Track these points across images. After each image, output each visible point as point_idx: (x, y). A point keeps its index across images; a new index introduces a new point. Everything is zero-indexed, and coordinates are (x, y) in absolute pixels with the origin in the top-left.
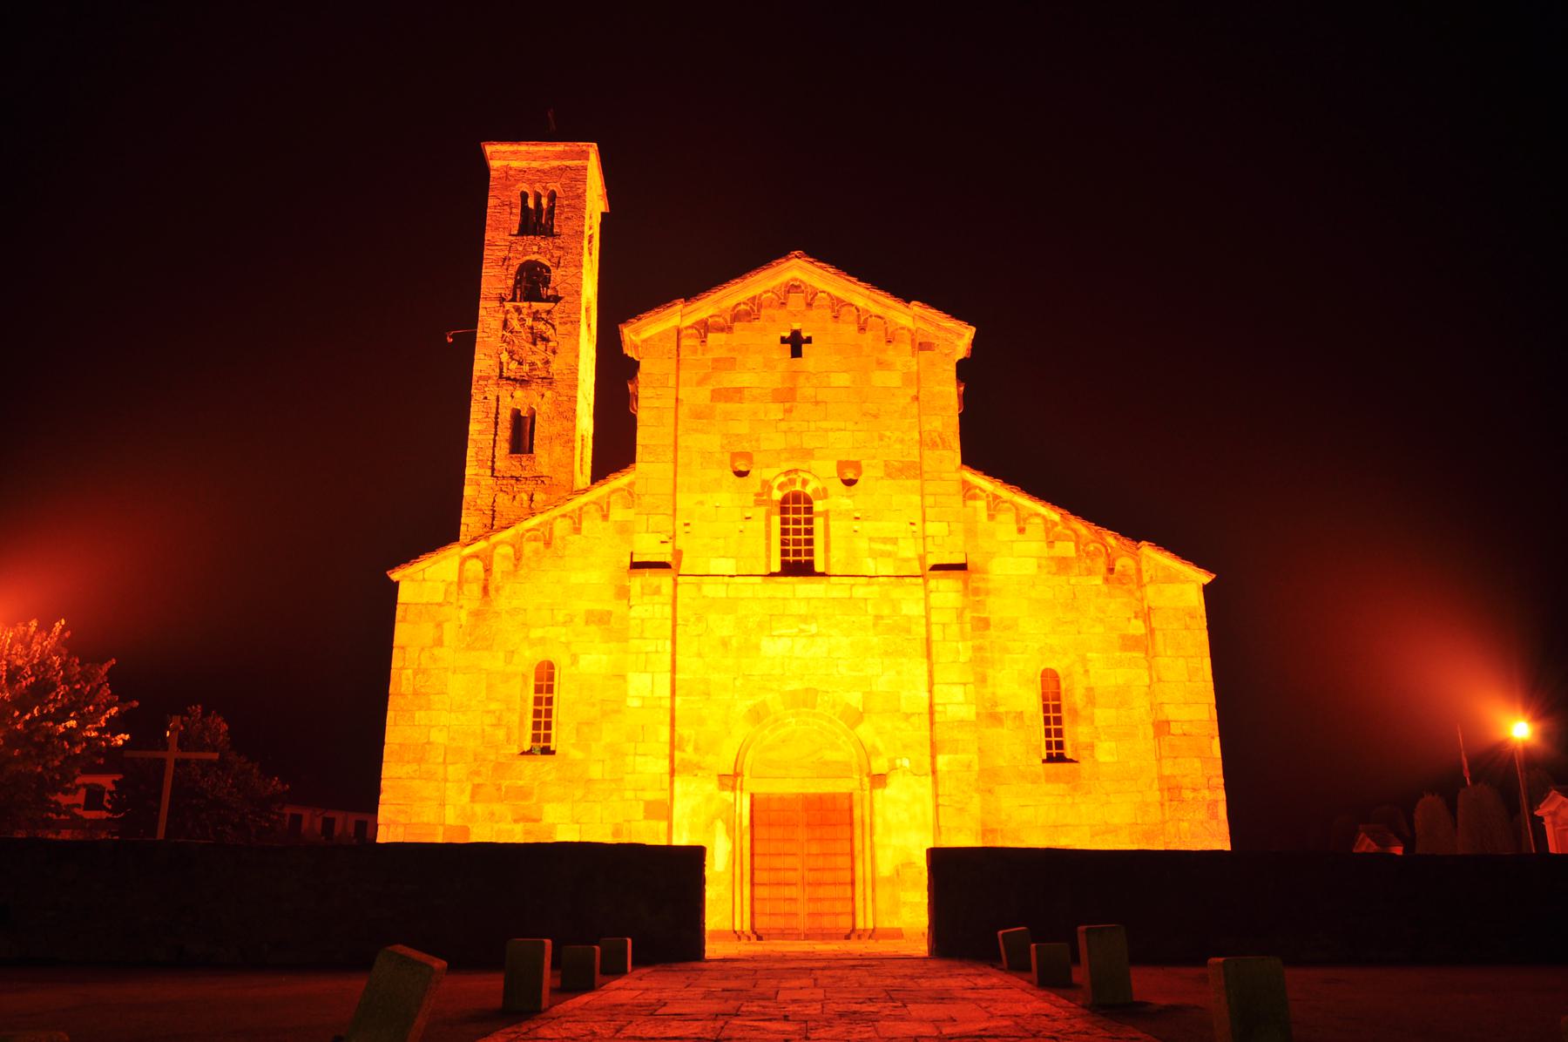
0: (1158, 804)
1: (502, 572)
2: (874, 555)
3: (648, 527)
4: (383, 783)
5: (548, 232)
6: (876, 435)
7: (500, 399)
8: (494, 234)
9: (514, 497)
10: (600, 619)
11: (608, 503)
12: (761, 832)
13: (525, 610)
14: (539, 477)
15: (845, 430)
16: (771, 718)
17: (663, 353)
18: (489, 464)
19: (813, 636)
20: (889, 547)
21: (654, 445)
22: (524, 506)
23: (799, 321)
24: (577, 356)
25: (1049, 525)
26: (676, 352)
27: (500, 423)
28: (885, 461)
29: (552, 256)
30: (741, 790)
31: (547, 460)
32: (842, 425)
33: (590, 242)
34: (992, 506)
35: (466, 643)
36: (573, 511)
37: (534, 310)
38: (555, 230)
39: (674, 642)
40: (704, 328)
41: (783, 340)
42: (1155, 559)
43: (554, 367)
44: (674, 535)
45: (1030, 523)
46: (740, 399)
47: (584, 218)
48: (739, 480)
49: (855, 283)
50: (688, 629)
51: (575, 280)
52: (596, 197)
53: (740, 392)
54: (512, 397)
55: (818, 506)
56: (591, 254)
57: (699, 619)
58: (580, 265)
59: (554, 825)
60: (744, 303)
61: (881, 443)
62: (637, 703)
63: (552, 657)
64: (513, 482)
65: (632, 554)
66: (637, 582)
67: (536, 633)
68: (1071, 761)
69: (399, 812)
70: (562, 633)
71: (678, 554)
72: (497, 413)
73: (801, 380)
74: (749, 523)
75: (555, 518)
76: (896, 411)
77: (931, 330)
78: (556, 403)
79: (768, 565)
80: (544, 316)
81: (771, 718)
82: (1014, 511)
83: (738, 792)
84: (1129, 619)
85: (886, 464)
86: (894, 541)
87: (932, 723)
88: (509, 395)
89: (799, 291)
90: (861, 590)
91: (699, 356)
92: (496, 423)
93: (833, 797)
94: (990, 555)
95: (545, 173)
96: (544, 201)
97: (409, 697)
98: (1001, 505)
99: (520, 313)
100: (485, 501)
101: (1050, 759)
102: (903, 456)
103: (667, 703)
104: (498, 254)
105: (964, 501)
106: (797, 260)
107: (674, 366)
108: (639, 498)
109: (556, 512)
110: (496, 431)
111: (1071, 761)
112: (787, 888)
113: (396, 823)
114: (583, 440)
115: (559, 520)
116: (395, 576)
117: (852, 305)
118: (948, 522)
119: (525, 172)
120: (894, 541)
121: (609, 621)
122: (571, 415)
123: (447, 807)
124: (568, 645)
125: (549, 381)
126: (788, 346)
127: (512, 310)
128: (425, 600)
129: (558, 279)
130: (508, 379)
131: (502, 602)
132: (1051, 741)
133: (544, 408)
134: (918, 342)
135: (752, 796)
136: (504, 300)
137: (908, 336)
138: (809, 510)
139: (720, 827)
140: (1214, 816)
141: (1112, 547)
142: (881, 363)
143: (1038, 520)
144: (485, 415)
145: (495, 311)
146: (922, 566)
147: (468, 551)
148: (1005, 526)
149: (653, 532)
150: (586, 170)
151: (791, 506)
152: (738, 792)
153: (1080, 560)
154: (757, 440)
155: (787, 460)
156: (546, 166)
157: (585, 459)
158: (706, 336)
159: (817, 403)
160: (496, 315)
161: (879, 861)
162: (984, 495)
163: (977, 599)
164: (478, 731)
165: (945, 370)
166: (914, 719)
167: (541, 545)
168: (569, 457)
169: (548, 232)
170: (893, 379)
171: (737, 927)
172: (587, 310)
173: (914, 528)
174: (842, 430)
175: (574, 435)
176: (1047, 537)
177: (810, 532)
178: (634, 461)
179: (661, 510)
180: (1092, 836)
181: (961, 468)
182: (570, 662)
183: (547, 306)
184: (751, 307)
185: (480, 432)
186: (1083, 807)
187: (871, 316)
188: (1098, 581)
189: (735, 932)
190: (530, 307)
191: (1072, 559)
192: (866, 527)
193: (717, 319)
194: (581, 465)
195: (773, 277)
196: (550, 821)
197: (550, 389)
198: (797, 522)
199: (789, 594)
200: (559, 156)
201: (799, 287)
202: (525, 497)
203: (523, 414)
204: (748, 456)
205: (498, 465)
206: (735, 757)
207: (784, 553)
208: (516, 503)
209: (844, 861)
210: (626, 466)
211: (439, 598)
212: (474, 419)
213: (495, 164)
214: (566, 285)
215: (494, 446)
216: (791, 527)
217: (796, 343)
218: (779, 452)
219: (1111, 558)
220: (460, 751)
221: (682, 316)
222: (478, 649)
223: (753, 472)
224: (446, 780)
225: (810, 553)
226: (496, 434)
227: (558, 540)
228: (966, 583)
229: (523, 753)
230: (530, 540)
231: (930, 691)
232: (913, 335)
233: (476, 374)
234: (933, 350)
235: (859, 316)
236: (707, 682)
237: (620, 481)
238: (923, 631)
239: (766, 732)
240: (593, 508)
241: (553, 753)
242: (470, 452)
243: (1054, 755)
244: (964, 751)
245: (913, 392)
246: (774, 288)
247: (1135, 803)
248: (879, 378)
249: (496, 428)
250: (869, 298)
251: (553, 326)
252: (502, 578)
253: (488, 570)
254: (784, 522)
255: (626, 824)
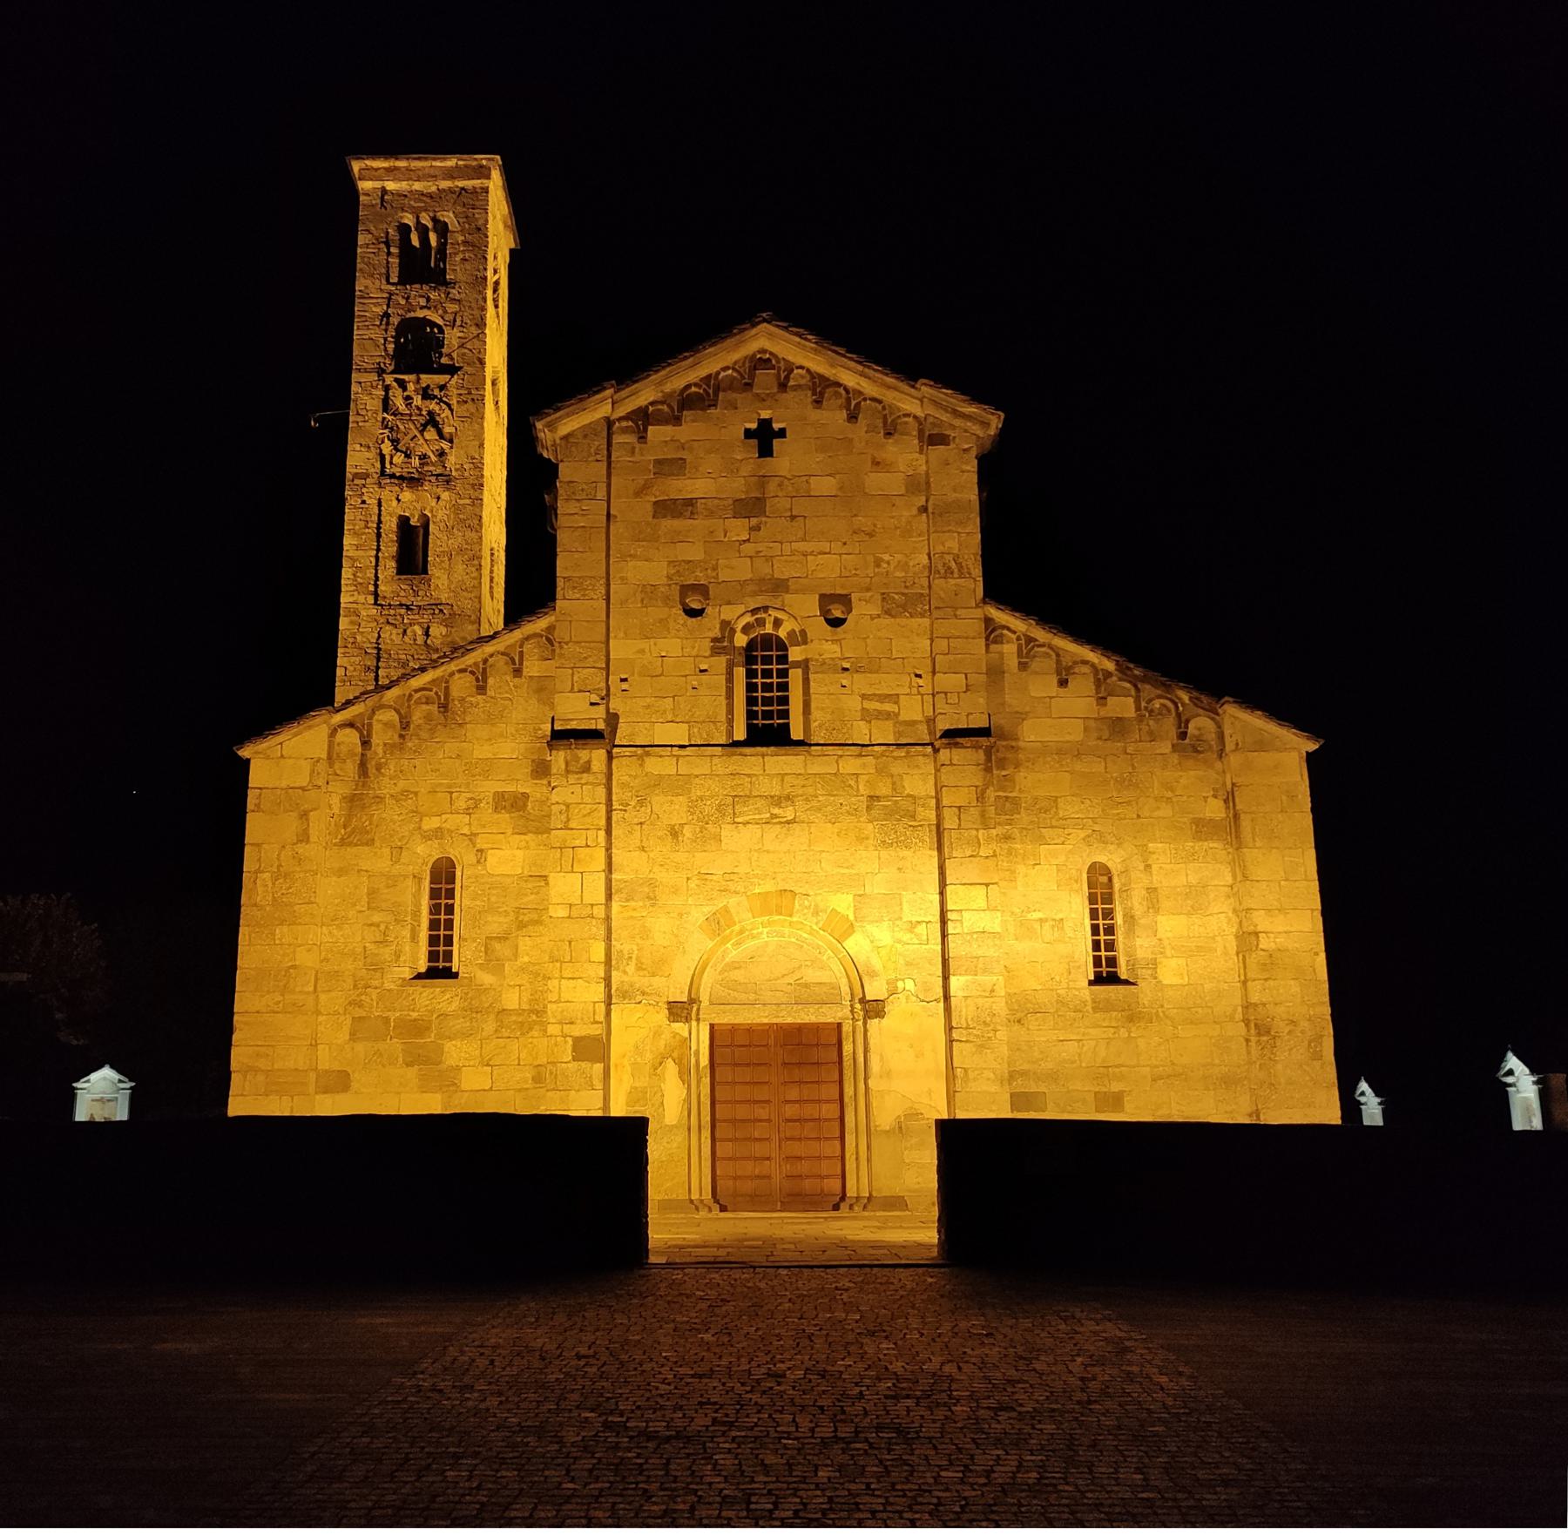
0: (1242, 1040)
1: (385, 745)
2: (867, 716)
3: (573, 685)
4: (236, 1018)
5: (438, 278)
6: (870, 559)
7: (383, 504)
8: (368, 282)
9: (405, 631)
10: (513, 803)
11: (521, 653)
12: (724, 1074)
13: (416, 794)
14: (436, 605)
15: (829, 553)
16: (737, 928)
17: (590, 455)
18: (372, 588)
19: (788, 822)
20: (888, 707)
21: (580, 578)
22: (418, 642)
23: (769, 408)
24: (482, 446)
25: (1101, 676)
26: (606, 452)
27: (383, 535)
28: (884, 594)
29: (445, 312)
30: (698, 1020)
31: (446, 583)
32: (826, 546)
33: (495, 290)
34: (1025, 651)
35: (339, 837)
36: (476, 664)
37: (424, 385)
38: (448, 277)
39: (609, 832)
40: (642, 419)
41: (749, 434)
42: (1241, 721)
43: (452, 460)
44: (608, 695)
45: (1074, 673)
46: (692, 513)
47: (486, 259)
48: (692, 621)
49: (844, 356)
50: (626, 815)
51: (477, 343)
52: (501, 226)
53: (692, 505)
54: (399, 500)
55: (795, 654)
56: (497, 307)
57: (641, 803)
58: (481, 324)
59: (458, 1068)
60: (696, 385)
61: (876, 570)
62: (562, 912)
63: (453, 853)
64: (403, 611)
65: (553, 718)
66: (559, 758)
67: (430, 823)
68: (1127, 982)
69: (258, 1055)
70: (460, 822)
71: (613, 719)
72: (380, 522)
73: (772, 487)
74: (704, 677)
75: (452, 674)
76: (896, 528)
77: (945, 417)
78: (457, 508)
79: (730, 733)
80: (436, 392)
81: (737, 928)
82: (1054, 656)
83: (694, 1023)
84: (1205, 798)
85: (885, 597)
86: (894, 698)
87: (944, 935)
88: (393, 498)
89: (769, 365)
90: (850, 765)
91: (637, 458)
92: (379, 535)
93: (816, 1029)
94: (1021, 716)
95: (432, 197)
96: (433, 238)
97: (268, 909)
98: (1036, 649)
99: (405, 389)
100: (367, 636)
101: (1099, 980)
102: (906, 587)
103: (600, 912)
104: (374, 309)
105: (987, 646)
106: (765, 324)
107: (604, 472)
108: (561, 648)
109: (453, 667)
110: (378, 546)
111: (1127, 982)
112: (757, 1145)
113: (256, 1070)
114: (492, 554)
115: (457, 676)
116: (244, 753)
117: (839, 385)
118: (966, 674)
119: (405, 196)
120: (894, 698)
121: (525, 805)
122: (475, 524)
123: (320, 1047)
124: (472, 837)
125: (446, 480)
126: (754, 442)
127: (395, 384)
128: (284, 784)
129: (455, 343)
130: (392, 476)
131: (385, 786)
132: (1099, 940)
133: (441, 515)
134: (927, 434)
135: (712, 1026)
136: (383, 371)
137: (913, 426)
138: (783, 659)
139: (671, 1068)
140: (1317, 1056)
141: (1183, 705)
142: (878, 463)
143: (1086, 669)
144: (363, 524)
145: (372, 387)
146: (931, 732)
147: (338, 718)
148: (1043, 685)
149: (580, 691)
150: (487, 192)
151: (758, 653)
152: (694, 1023)
153: (1141, 721)
154: (715, 569)
155: (754, 594)
156: (434, 189)
157: (495, 580)
158: (646, 430)
159: (793, 518)
160: (374, 391)
161: (875, 1111)
162: (1014, 637)
163: (1004, 773)
164: (359, 950)
165: (963, 472)
166: (921, 929)
167: (434, 708)
168: (474, 578)
169: (438, 278)
170: (892, 483)
171: (695, 1196)
172: (494, 383)
173: (921, 682)
174: (826, 553)
175: (480, 550)
176: (1097, 693)
177: (784, 687)
178: (554, 599)
179: (590, 661)
180: (1154, 1080)
181: (984, 601)
182: (474, 860)
183: (441, 379)
184: (705, 390)
185: (358, 547)
186: (1141, 1043)
187: (865, 399)
188: (1165, 747)
189: (692, 1201)
190: (418, 380)
191: (1129, 719)
192: (861, 683)
193: (660, 407)
194: (491, 587)
195: (737, 346)
196: (452, 1062)
197: (448, 489)
198: (767, 674)
199: (757, 770)
200: (450, 174)
201: (769, 360)
202: (419, 630)
203: (414, 522)
204: (702, 590)
205: (382, 588)
206: (689, 980)
207: (751, 715)
208: (406, 639)
209: (831, 1110)
210: (544, 606)
211: (303, 781)
212: (349, 530)
213: (365, 185)
214: (466, 351)
215: (377, 565)
216: (759, 681)
217: (764, 438)
218: (743, 584)
219: (1183, 719)
220: (336, 974)
221: (613, 404)
222: (356, 845)
223: (709, 610)
224: (318, 1013)
225: (785, 714)
226: (378, 550)
227: (456, 702)
228: (988, 752)
229: (419, 976)
230: (418, 702)
231: (942, 893)
232: (921, 424)
233: (350, 470)
234: (948, 444)
235: (848, 400)
236: (652, 883)
237: (540, 624)
238: (932, 815)
239: (729, 945)
240: (501, 661)
241: (456, 976)
242: (346, 573)
243: (1105, 975)
244: (985, 971)
245: (921, 501)
246: (735, 363)
247: (1211, 1038)
248: (875, 481)
249: (378, 541)
250: (862, 374)
251: (449, 406)
252: (385, 752)
253: (366, 743)
254: (751, 674)
255: (549, 1067)
